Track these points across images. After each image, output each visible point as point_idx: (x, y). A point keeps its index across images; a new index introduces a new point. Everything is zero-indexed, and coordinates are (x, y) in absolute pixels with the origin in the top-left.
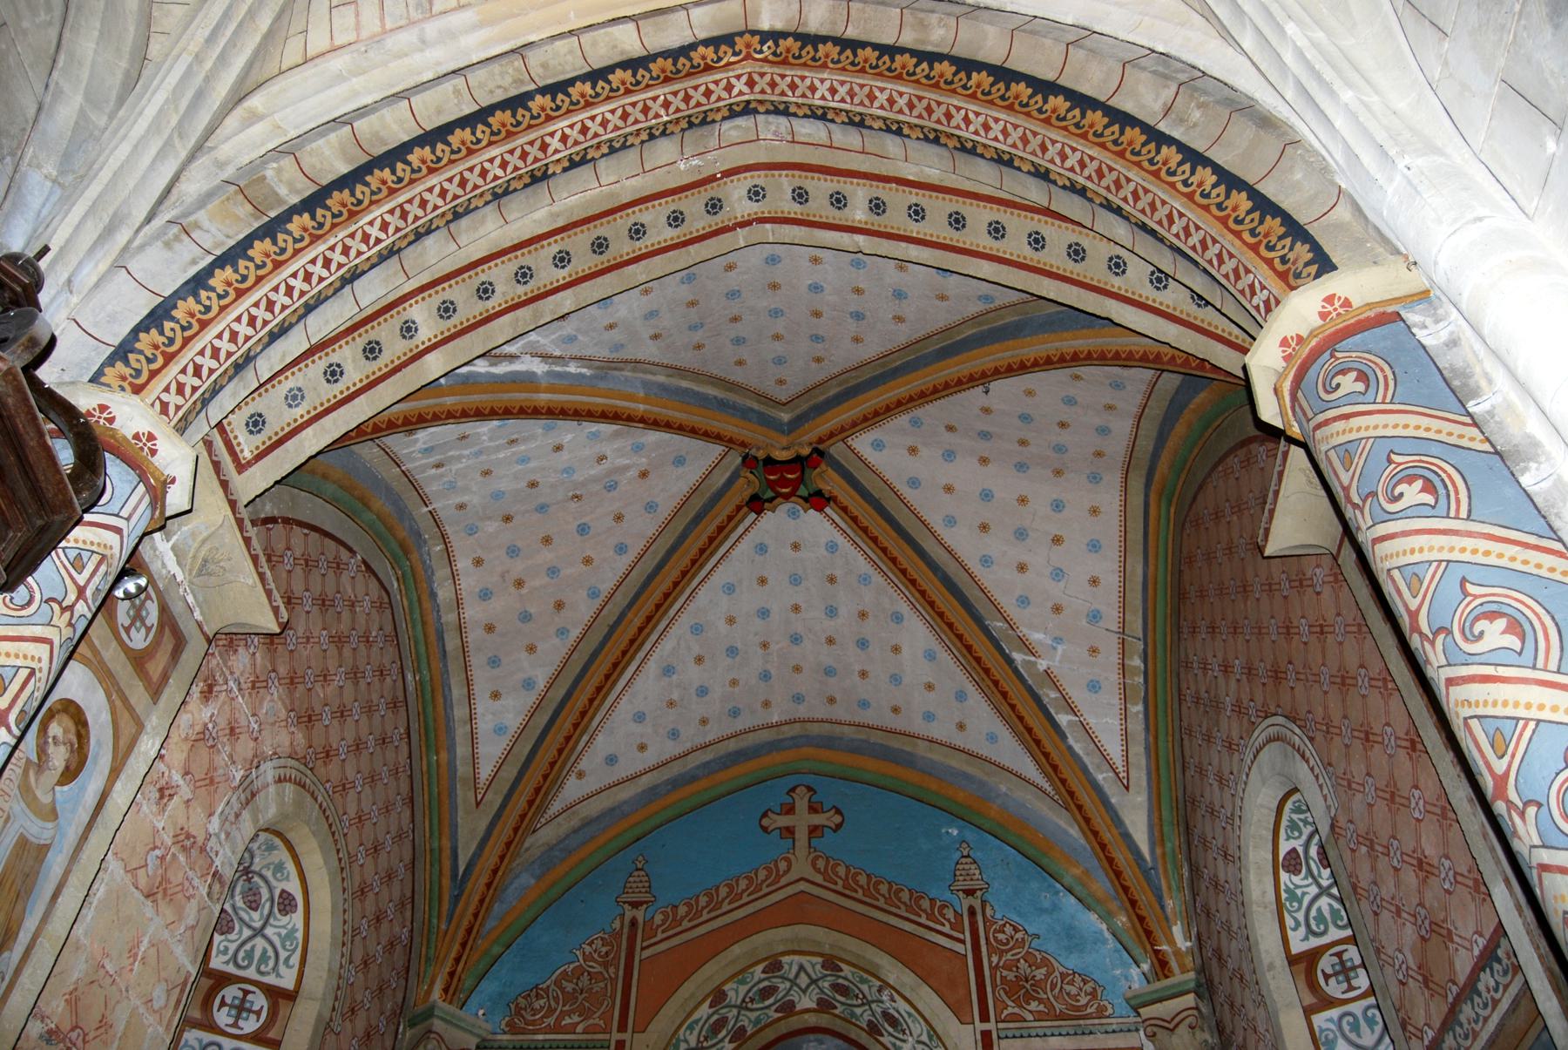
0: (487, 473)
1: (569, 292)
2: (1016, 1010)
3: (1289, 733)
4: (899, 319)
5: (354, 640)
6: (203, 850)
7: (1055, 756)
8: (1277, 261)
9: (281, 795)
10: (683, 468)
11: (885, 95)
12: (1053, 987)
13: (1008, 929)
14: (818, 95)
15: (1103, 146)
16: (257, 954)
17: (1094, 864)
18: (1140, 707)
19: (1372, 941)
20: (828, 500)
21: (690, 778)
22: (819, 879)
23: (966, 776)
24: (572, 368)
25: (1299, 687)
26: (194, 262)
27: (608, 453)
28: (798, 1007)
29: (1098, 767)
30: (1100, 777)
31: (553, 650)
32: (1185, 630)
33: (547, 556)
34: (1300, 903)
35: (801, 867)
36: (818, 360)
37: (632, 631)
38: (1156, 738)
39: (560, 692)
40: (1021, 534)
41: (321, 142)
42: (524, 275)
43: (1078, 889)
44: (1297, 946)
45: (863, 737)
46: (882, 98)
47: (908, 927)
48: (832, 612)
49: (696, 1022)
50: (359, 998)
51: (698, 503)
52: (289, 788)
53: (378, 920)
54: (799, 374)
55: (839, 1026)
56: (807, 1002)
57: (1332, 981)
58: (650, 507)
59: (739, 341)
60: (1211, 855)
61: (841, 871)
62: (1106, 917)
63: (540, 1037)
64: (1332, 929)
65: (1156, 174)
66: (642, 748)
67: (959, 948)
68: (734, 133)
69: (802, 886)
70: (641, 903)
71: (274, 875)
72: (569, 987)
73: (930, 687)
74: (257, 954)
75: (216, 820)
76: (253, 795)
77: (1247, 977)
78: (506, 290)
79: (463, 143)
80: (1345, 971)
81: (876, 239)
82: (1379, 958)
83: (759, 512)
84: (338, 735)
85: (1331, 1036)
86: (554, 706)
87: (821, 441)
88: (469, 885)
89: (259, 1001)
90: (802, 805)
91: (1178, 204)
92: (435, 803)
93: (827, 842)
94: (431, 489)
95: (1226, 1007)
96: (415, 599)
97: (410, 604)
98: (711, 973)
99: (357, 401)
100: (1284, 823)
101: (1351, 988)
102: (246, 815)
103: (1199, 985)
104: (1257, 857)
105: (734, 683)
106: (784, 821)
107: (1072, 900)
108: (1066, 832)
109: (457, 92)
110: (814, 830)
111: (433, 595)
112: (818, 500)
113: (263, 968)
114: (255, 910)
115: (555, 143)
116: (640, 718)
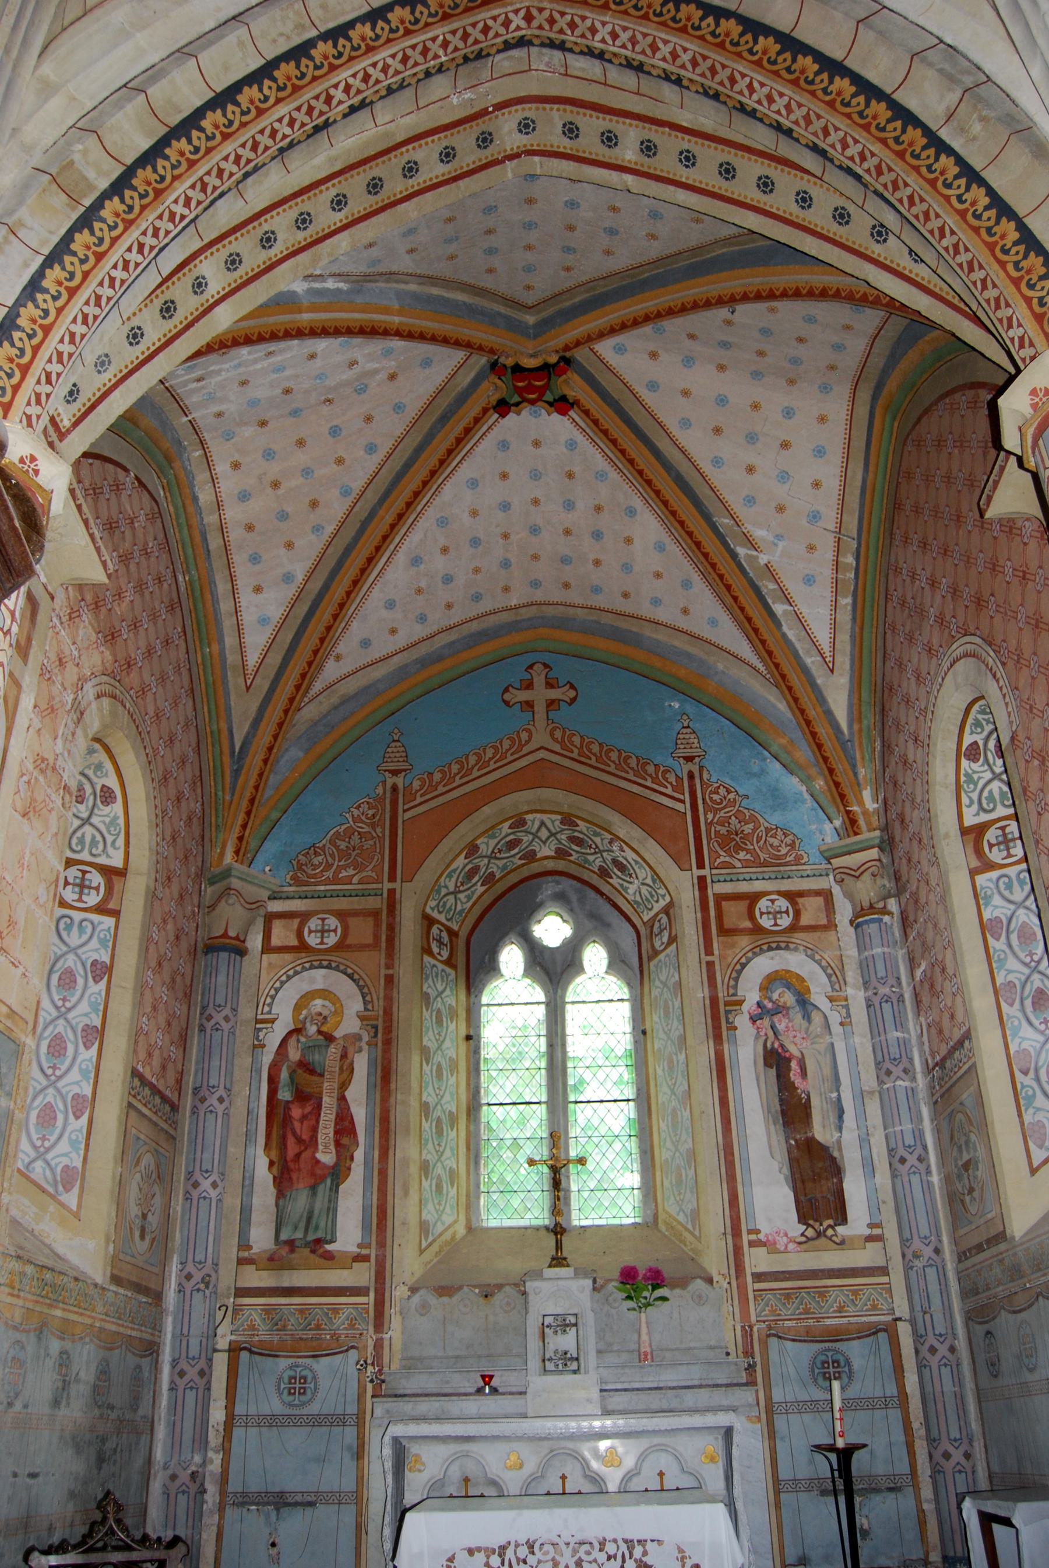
0: (244, 383)
1: (346, 233)
2: (727, 859)
3: (984, 654)
4: (653, 237)
5: (136, 554)
6: (54, 769)
7: (772, 645)
8: (1035, 301)
9: (100, 709)
10: (428, 373)
11: (669, 48)
12: (759, 839)
13: (722, 791)
14: (598, 37)
15: (884, 142)
16: (88, 839)
17: (797, 734)
18: (849, 600)
19: (1034, 833)
20: (572, 405)
21: (437, 658)
22: (557, 748)
23: (689, 656)
24: (331, 284)
25: (998, 618)
26: (26, 265)
27: (359, 359)
28: (539, 856)
29: (808, 652)
30: (808, 661)
31: (310, 546)
32: (898, 537)
33: (301, 458)
34: (976, 784)
35: (541, 737)
36: (568, 269)
37: (384, 527)
38: (862, 629)
39: (316, 586)
40: (752, 438)
41: (120, 115)
42: (304, 221)
43: (783, 756)
44: (969, 821)
45: (594, 618)
46: (665, 50)
47: (635, 789)
48: (569, 505)
49: (454, 871)
50: (172, 867)
51: (444, 403)
52: (106, 701)
53: (178, 800)
54: (546, 281)
55: (573, 870)
56: (547, 851)
57: (995, 849)
58: (398, 408)
59: (491, 251)
60: (902, 738)
61: (577, 740)
62: (807, 780)
63: (322, 888)
64: (999, 807)
65: (932, 183)
66: (393, 631)
67: (679, 807)
68: (506, 64)
69: (542, 754)
70: (400, 771)
71: (95, 773)
72: (343, 845)
73: (658, 575)
74: (88, 839)
75: (59, 741)
76: (82, 714)
77: (925, 841)
78: (287, 237)
79: (252, 102)
80: (1005, 842)
81: (644, 180)
82: (1037, 848)
83: (503, 415)
84: (134, 645)
85: (989, 893)
86: (312, 596)
87: (567, 348)
88: (248, 760)
89: (96, 878)
90: (539, 680)
91: (951, 221)
92: (211, 691)
93: (564, 714)
94: (191, 401)
95: (904, 861)
96: (180, 504)
97: (176, 509)
98: (464, 832)
99: (156, 359)
100: (970, 720)
101: (1009, 856)
102: (79, 732)
103: (882, 841)
104: (944, 747)
105: (477, 570)
106: (524, 696)
107: (778, 765)
108: (774, 706)
109: (241, 44)
110: (551, 704)
111: (195, 499)
112: (562, 405)
113: (94, 851)
114: (81, 803)
115: (338, 94)
116: (390, 605)
